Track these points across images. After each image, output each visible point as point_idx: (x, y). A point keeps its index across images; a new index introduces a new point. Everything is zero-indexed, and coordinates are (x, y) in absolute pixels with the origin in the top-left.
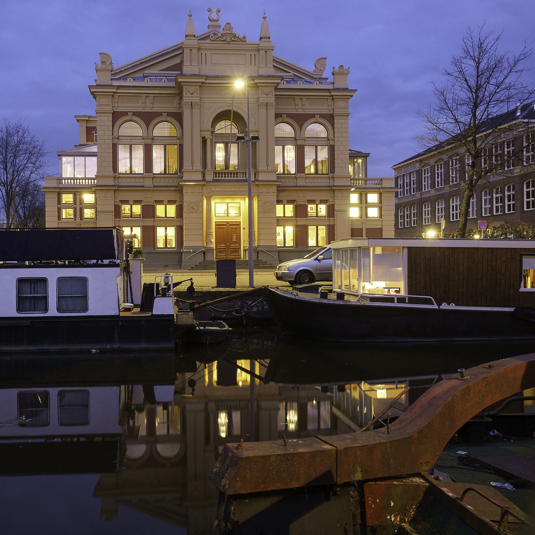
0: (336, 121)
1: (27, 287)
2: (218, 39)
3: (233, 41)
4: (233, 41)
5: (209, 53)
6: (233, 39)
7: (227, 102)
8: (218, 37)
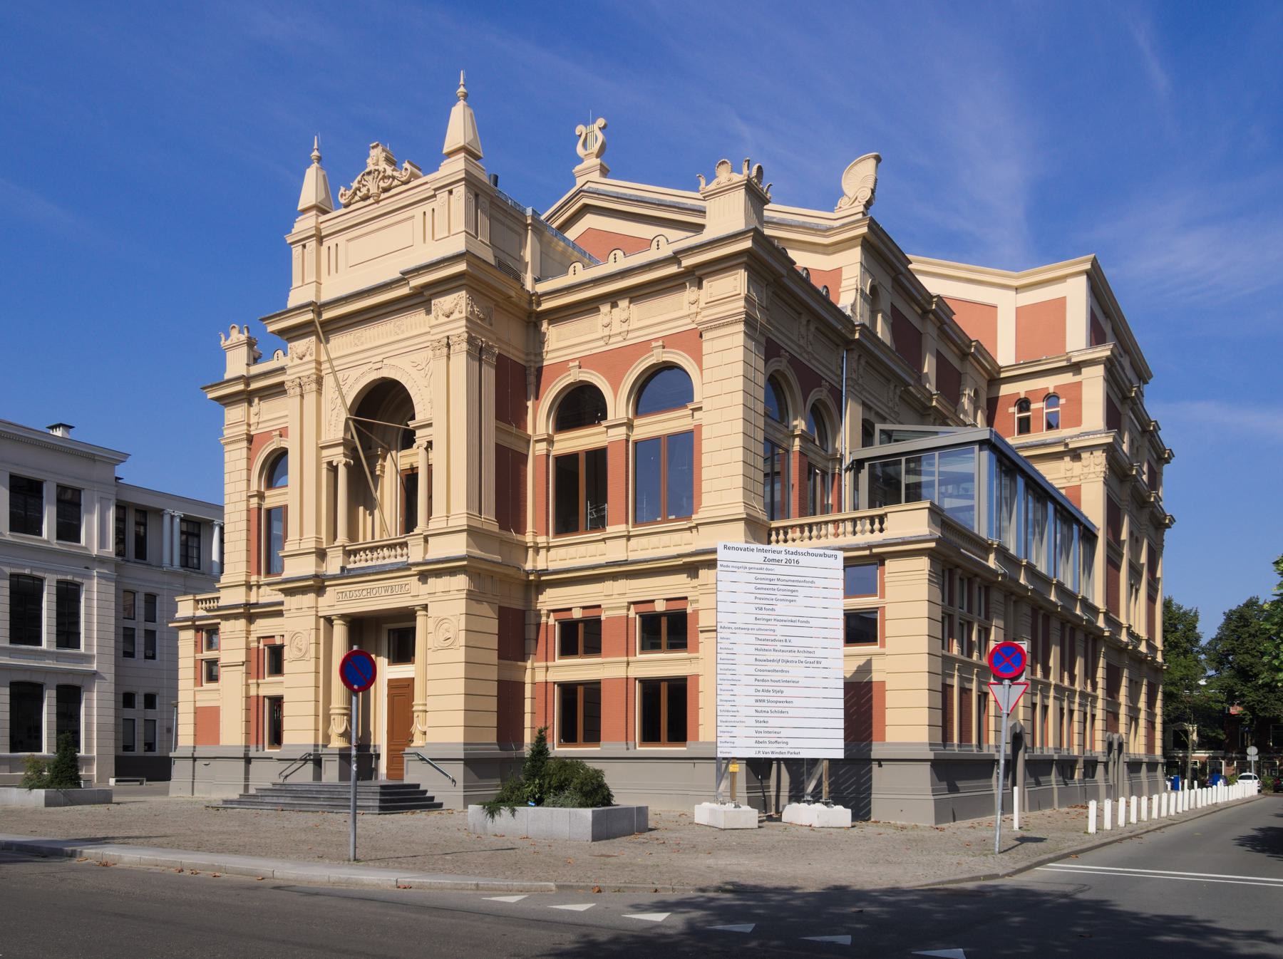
0: (706, 347)
2: (357, 198)
3: (386, 190)
4: (386, 190)
5: (341, 239)
6: (382, 184)
7: (374, 360)
8: (355, 194)
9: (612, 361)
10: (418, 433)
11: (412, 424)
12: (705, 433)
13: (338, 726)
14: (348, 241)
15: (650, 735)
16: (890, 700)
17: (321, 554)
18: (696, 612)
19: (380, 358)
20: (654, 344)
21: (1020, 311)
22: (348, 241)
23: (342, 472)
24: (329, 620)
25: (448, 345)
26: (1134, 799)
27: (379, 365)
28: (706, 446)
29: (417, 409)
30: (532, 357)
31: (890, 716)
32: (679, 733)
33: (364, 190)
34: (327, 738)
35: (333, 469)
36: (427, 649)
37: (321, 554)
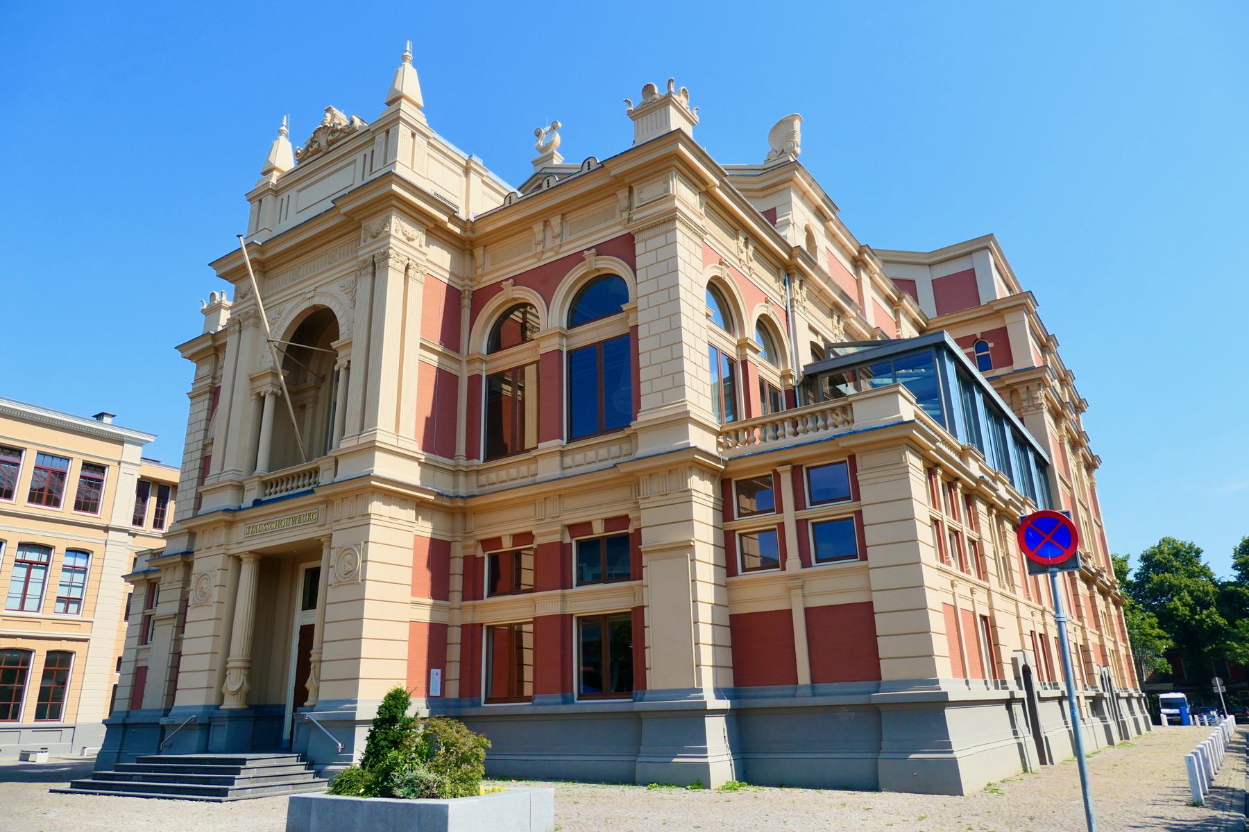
0: (639, 248)
1: (500, 585)
3: (330, 143)
5: (292, 192)
9: (543, 279)
10: (341, 354)
11: (334, 344)
12: (642, 332)
13: (235, 681)
14: (52, 791)
15: (592, 685)
16: (407, 576)
17: (240, 487)
18: (638, 531)
19: (312, 287)
20: (586, 253)
21: (936, 283)
22: (299, 191)
23: (269, 403)
24: (238, 559)
25: (407, 267)
26: (1041, 577)
27: (309, 296)
28: (643, 346)
29: (342, 330)
30: (467, 282)
31: (403, 650)
32: (56, 715)
33: (315, 146)
34: (221, 697)
35: (261, 400)
36: (327, 585)
37: (240, 487)
